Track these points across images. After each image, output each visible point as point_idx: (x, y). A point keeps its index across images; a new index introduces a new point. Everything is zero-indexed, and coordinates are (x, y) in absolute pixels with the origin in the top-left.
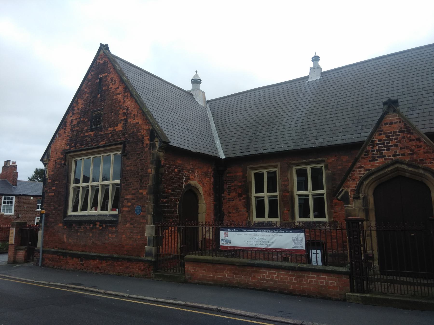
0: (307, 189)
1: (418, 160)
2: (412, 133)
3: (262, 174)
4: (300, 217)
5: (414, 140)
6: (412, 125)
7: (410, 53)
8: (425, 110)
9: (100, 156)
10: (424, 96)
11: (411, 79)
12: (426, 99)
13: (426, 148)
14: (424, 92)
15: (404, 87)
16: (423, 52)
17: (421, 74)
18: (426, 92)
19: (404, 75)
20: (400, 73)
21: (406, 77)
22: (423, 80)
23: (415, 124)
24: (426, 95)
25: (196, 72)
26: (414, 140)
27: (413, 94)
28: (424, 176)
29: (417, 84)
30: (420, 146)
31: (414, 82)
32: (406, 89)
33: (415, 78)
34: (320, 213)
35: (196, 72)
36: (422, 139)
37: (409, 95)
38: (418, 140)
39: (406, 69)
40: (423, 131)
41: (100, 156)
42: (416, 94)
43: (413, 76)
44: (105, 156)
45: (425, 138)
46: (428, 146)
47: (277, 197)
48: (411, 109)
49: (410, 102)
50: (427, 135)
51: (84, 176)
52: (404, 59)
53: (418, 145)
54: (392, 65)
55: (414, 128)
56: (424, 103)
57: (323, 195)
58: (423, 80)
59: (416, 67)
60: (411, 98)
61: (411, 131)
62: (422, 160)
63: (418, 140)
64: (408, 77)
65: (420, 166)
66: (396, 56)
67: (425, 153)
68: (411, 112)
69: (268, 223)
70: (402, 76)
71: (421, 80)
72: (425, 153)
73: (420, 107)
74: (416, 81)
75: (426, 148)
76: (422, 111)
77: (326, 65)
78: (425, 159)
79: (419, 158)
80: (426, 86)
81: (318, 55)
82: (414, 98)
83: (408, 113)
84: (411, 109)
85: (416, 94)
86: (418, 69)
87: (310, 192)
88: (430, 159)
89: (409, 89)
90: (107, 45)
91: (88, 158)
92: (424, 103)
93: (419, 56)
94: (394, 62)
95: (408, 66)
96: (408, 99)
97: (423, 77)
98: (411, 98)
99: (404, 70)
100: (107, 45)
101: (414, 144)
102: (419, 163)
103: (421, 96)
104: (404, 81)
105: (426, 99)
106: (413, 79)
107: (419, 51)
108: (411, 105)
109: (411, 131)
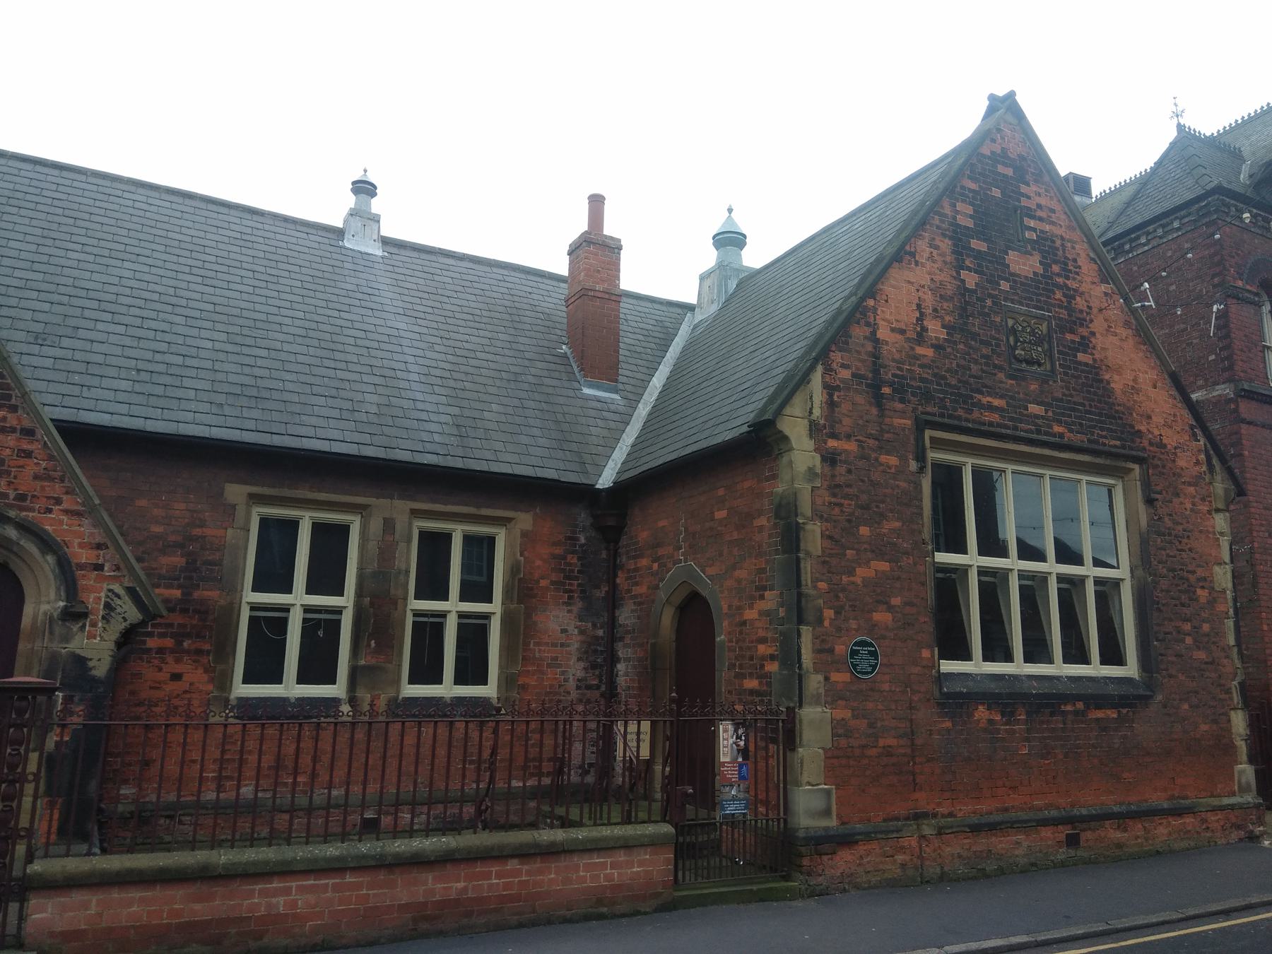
0: (288, 589)
1: (12, 494)
2: (14, 409)
3: (447, 538)
4: (412, 681)
5: (13, 430)
6: (20, 384)
7: (83, 178)
8: (78, 356)
9: (1079, 481)
10: (87, 313)
11: (62, 253)
12: (91, 325)
13: (44, 464)
14: (88, 304)
15: (36, 266)
16: (119, 193)
17: (95, 251)
18: (95, 304)
19: (46, 233)
20: (34, 223)
21: (50, 242)
22: (97, 268)
23: (31, 385)
24: (94, 315)
25: (730, 210)
26: (13, 430)
27: (55, 298)
28: (15, 549)
29: (76, 273)
30: (28, 454)
31: (70, 263)
32: (40, 276)
33: (75, 255)
34: (317, 666)
35: (730, 210)
36: (40, 432)
37: (43, 296)
38: (29, 433)
39: (56, 219)
40: (49, 413)
41: (1041, 476)
42: (65, 299)
43: (71, 246)
44: (1061, 479)
45: (49, 433)
46: (51, 458)
47: (340, 613)
48: (36, 338)
49: (41, 317)
50: (57, 428)
51: (1056, 540)
52: (61, 188)
53: (24, 451)
54: (17, 187)
55: (25, 395)
56: (81, 333)
57: (338, 611)
58: (97, 268)
59: (87, 224)
60: (46, 307)
61: (13, 401)
62: (22, 497)
63: (29, 433)
64: (58, 243)
65: (12, 514)
66: (39, 168)
67: (36, 477)
68: (36, 349)
69: (302, 701)
70: (39, 232)
71: (91, 267)
72: (36, 477)
73: (66, 342)
74: (75, 264)
75: (44, 464)
76: (69, 354)
77: (402, 219)
78: (33, 496)
79: (16, 490)
80: (100, 286)
81: (371, 178)
82: (56, 308)
83: (25, 348)
84: (38, 339)
85: (65, 299)
86: (90, 233)
87: (298, 599)
88: (48, 498)
89: (48, 278)
90: (1011, 95)
91: (1033, 475)
92: (81, 333)
93: (105, 198)
94: (27, 181)
95: (67, 212)
96: (38, 306)
97: (99, 260)
98: (46, 307)
99: (50, 218)
100: (1011, 95)
101: (12, 444)
102: (11, 506)
103: (78, 312)
104: (42, 249)
105: (91, 325)
106: (70, 254)
107: (108, 183)
108: (39, 328)
109: (13, 401)
